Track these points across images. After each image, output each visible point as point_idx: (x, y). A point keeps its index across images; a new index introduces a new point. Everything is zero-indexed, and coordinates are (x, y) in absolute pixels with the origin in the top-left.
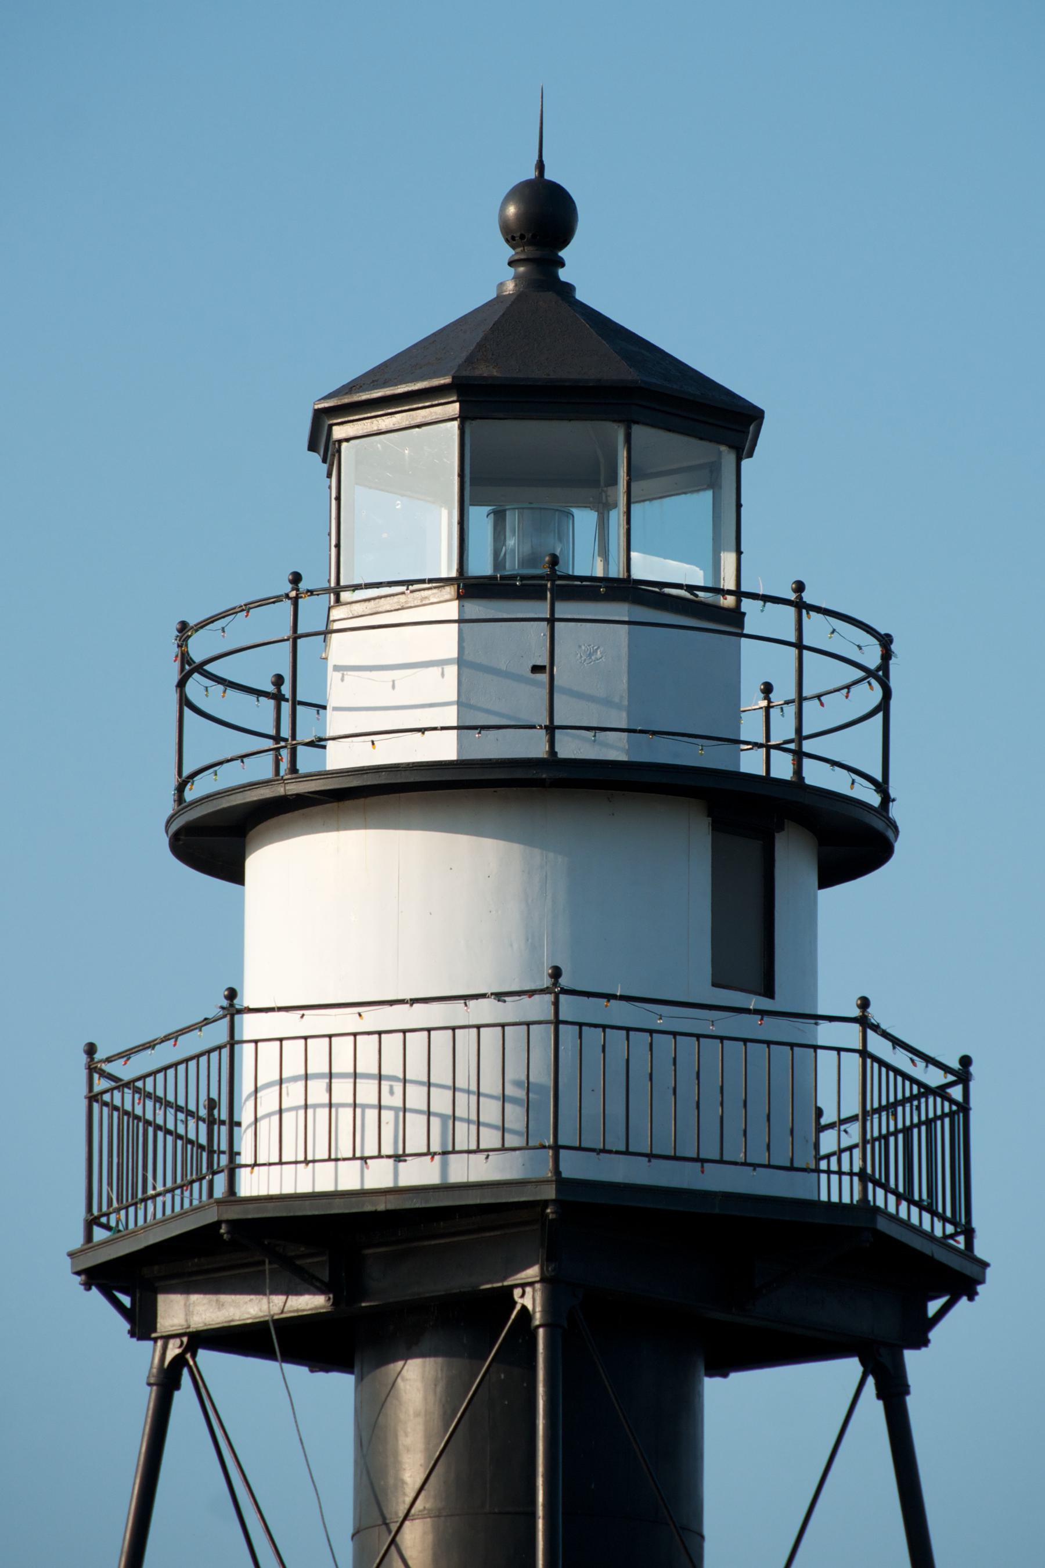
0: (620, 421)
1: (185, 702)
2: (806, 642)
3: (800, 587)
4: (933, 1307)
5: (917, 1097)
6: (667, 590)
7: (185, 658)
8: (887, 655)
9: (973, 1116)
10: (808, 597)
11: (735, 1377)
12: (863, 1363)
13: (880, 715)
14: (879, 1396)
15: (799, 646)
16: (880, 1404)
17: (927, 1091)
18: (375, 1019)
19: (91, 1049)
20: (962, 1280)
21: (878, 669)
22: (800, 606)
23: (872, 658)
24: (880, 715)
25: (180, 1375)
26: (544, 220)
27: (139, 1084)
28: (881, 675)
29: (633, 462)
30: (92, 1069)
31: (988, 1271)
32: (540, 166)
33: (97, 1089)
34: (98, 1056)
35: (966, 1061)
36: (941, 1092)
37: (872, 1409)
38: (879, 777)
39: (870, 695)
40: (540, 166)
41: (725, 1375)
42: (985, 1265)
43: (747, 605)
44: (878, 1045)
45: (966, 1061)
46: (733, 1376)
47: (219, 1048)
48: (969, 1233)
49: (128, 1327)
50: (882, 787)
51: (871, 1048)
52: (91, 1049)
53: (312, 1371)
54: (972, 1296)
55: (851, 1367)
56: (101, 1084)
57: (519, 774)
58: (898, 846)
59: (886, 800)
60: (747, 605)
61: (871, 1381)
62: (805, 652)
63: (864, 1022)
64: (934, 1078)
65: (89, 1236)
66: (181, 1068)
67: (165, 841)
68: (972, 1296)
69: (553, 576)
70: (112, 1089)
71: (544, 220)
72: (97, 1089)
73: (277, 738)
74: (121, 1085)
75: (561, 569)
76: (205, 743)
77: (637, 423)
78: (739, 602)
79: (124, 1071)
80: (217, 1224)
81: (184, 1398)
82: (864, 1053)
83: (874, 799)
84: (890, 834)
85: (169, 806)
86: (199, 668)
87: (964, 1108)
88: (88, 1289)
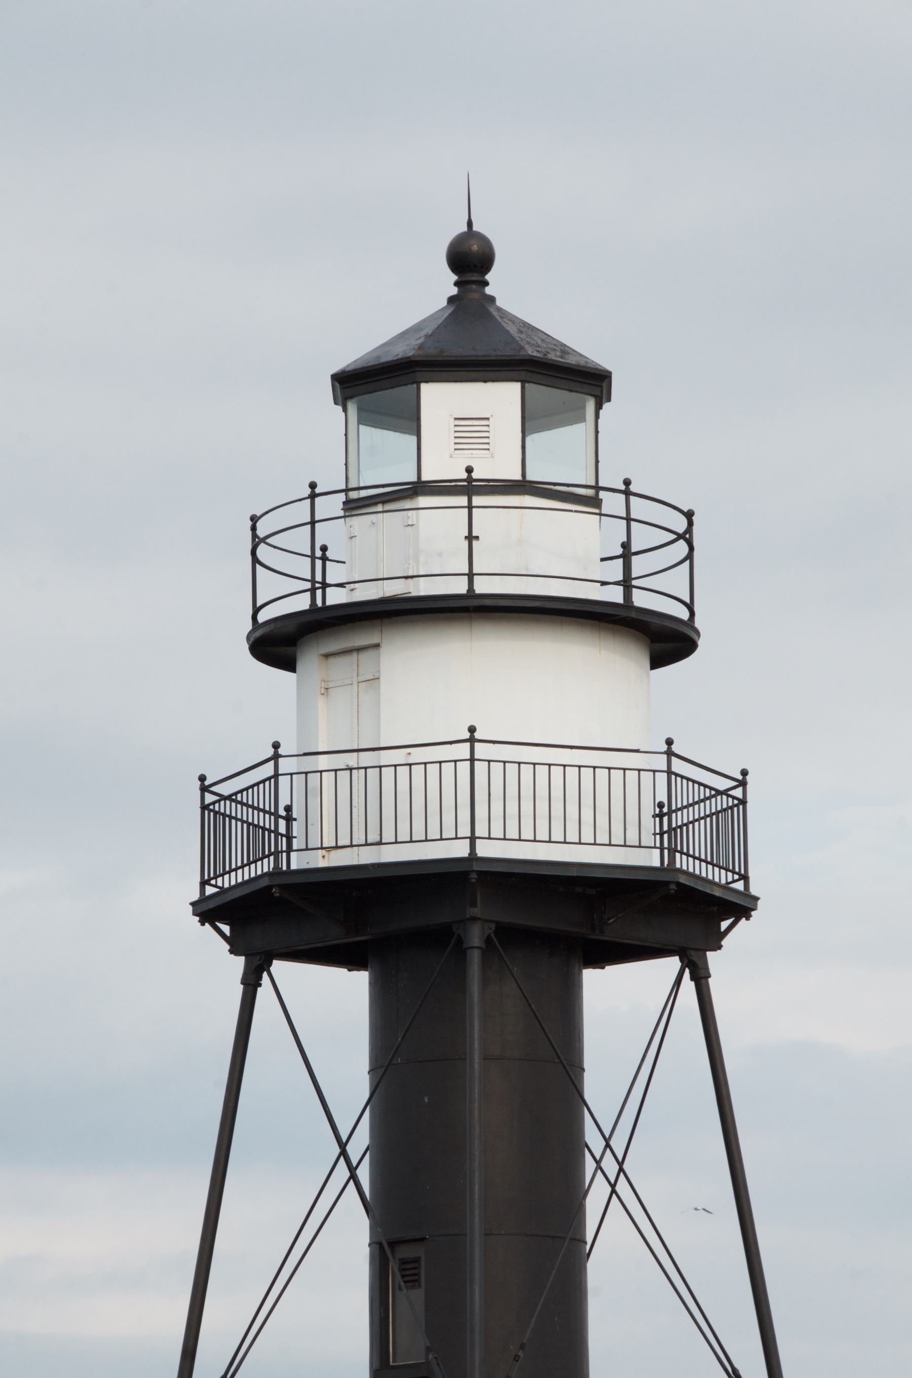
0: (592, 395)
1: (255, 561)
2: (633, 515)
3: (627, 482)
4: (724, 925)
5: (709, 798)
6: (552, 487)
7: (254, 535)
8: (690, 524)
9: (749, 806)
10: (633, 488)
11: (610, 969)
12: (681, 960)
13: (688, 562)
14: (692, 979)
15: (628, 519)
16: (693, 983)
17: (719, 793)
18: (351, 760)
19: (202, 778)
20: (741, 908)
21: (686, 532)
22: (627, 493)
23: (680, 525)
24: (688, 562)
25: (260, 978)
26: (470, 260)
27: (234, 797)
28: (687, 537)
29: (527, 406)
30: (204, 789)
31: (759, 902)
32: (470, 224)
33: (207, 802)
34: (207, 783)
35: (744, 773)
36: (725, 793)
37: (688, 986)
38: (688, 601)
39: (681, 548)
40: (470, 224)
41: (603, 968)
42: (757, 899)
43: (602, 494)
44: (678, 766)
45: (744, 773)
46: (607, 968)
47: (269, 779)
48: (745, 878)
49: (228, 947)
50: (690, 607)
51: (674, 769)
52: (202, 778)
53: (349, 970)
54: (748, 918)
55: (673, 964)
56: (209, 798)
57: (537, 604)
58: (700, 643)
59: (692, 614)
60: (602, 494)
61: (687, 970)
62: (633, 523)
63: (670, 753)
64: (722, 784)
65: (202, 890)
66: (261, 786)
67: (247, 646)
68: (748, 918)
69: (470, 480)
70: (219, 801)
71: (470, 260)
72: (207, 802)
73: (313, 581)
74: (223, 798)
75: (475, 475)
76: (269, 585)
77: (529, 382)
78: (597, 494)
79: (225, 789)
80: (269, 888)
81: (265, 992)
82: (669, 772)
83: (684, 614)
84: (694, 636)
85: (249, 627)
86: (680, 537)
87: (743, 802)
88: (203, 924)
